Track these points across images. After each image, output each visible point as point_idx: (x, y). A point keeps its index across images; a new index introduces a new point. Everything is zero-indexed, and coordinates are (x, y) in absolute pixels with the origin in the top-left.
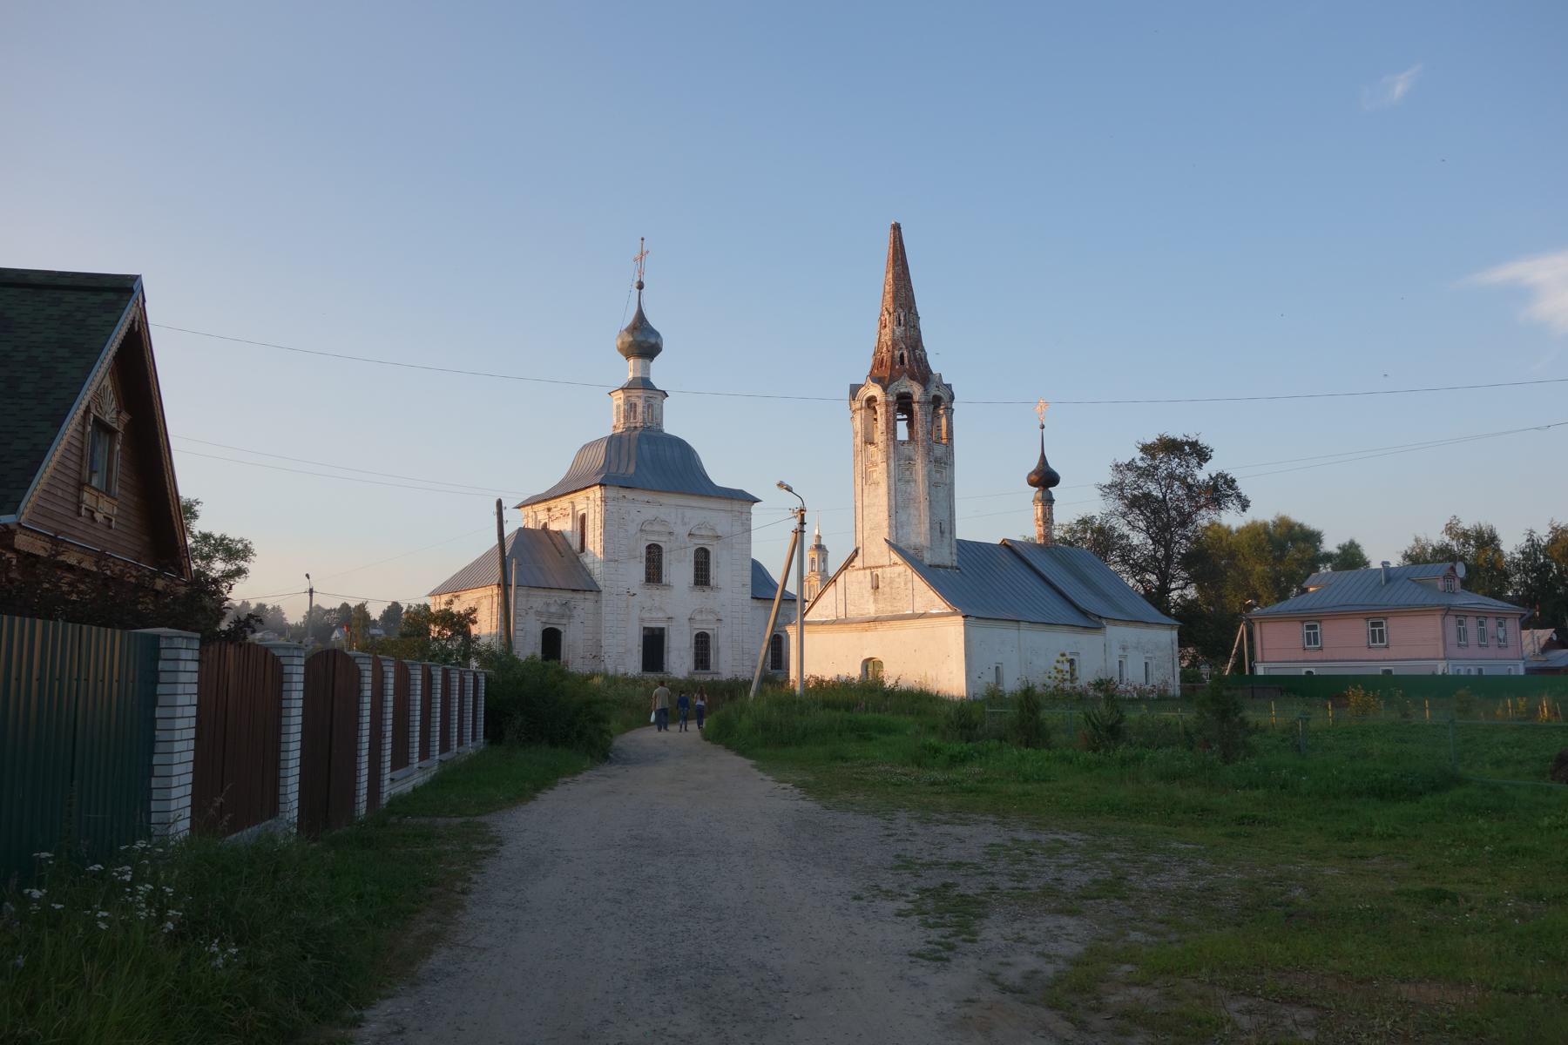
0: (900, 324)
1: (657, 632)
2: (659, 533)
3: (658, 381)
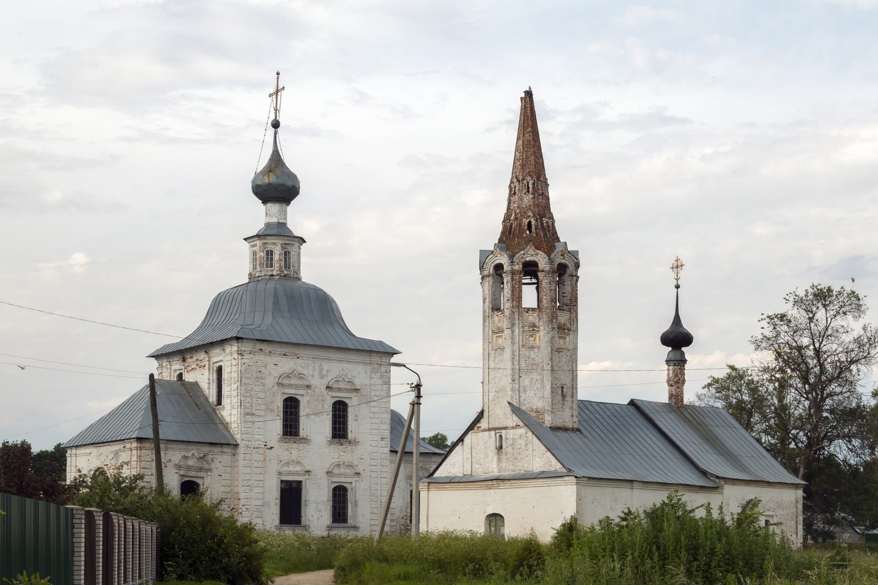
0: (528, 191)
1: (294, 485)
2: (296, 387)
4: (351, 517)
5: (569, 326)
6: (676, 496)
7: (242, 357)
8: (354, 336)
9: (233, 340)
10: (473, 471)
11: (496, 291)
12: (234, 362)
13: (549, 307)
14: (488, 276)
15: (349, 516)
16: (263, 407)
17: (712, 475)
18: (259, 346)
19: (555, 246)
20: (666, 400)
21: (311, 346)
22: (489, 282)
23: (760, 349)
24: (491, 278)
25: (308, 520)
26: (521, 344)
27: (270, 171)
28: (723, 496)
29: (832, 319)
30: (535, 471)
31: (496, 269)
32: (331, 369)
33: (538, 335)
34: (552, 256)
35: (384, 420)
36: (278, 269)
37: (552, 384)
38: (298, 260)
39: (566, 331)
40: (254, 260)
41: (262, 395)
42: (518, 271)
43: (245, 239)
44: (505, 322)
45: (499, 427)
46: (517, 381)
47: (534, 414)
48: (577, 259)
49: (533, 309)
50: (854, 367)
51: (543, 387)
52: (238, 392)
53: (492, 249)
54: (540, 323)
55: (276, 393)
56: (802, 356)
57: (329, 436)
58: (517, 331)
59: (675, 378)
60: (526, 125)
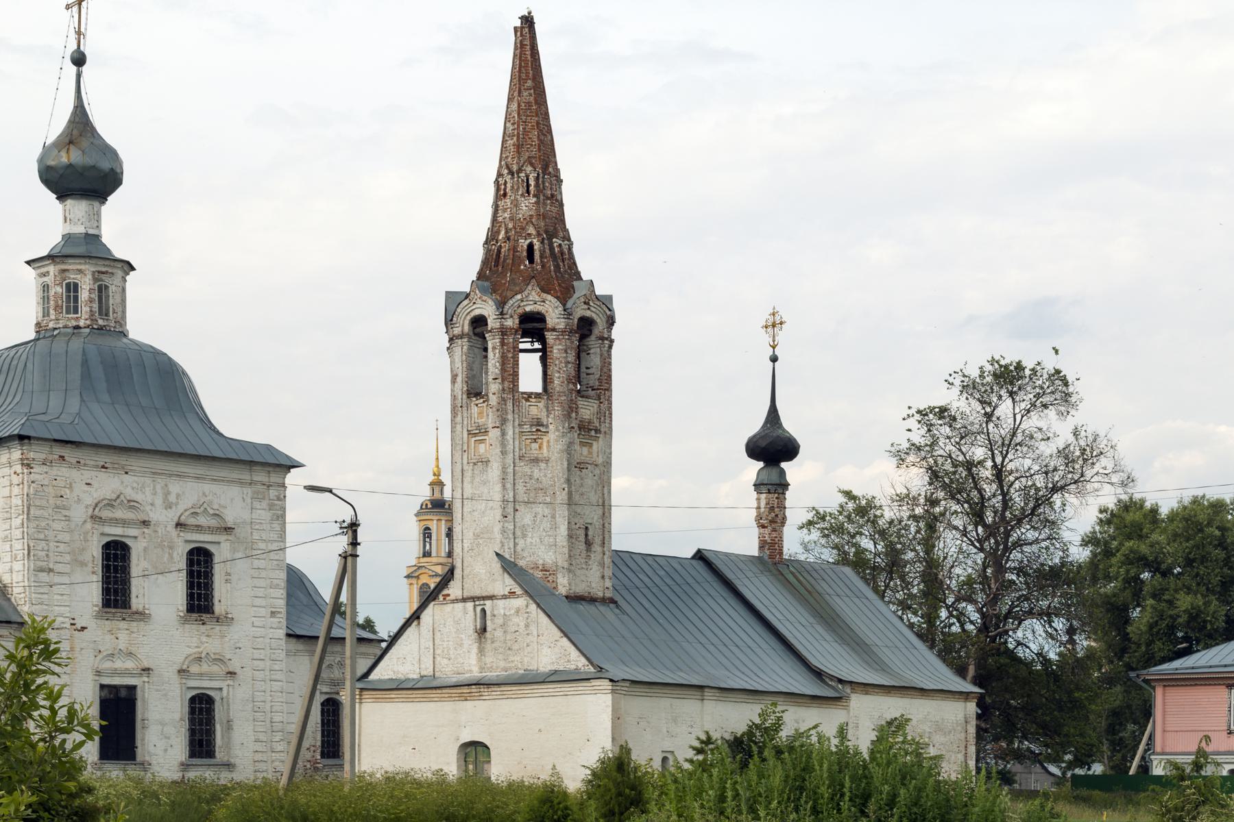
0: (528, 192)
1: (123, 693)
2: (124, 523)
3: (115, 238)
4: (219, 747)
5: (598, 425)
6: (774, 712)
7: (29, 471)
8: (221, 435)
9: (14, 440)
10: (437, 670)
11: (473, 362)
12: (16, 479)
13: (564, 392)
14: (461, 336)
15: (217, 746)
16: (68, 558)
17: (832, 677)
18: (59, 450)
19: (573, 287)
20: (754, 551)
21: (148, 452)
22: (462, 346)
23: (904, 466)
24: (466, 340)
25: (148, 752)
26: (517, 454)
27: (71, 142)
28: (849, 712)
29: (1022, 417)
30: (542, 669)
31: (475, 324)
32: (183, 492)
33: (545, 439)
34: (569, 304)
35: (275, 582)
36: (87, 317)
37: (569, 523)
38: (122, 300)
39: (593, 433)
40: (45, 299)
41: (66, 537)
42: (511, 329)
43: (28, 263)
44: (490, 417)
45: (480, 595)
46: (510, 518)
47: (539, 574)
48: (610, 310)
49: (538, 395)
50: (1057, 499)
51: (555, 527)
52: (23, 532)
53: (468, 290)
54: (550, 419)
55: (90, 534)
56: (974, 478)
57: (181, 608)
58: (510, 432)
59: (770, 513)
60: (523, 76)
